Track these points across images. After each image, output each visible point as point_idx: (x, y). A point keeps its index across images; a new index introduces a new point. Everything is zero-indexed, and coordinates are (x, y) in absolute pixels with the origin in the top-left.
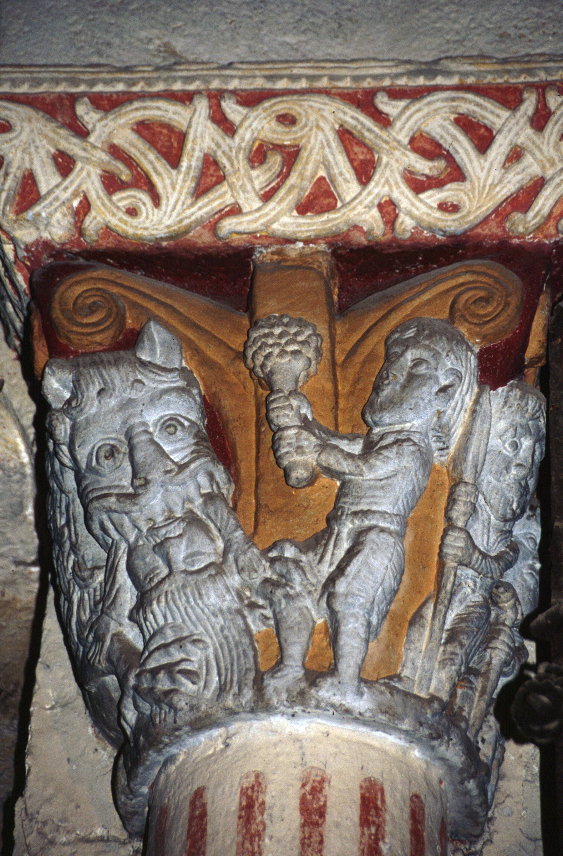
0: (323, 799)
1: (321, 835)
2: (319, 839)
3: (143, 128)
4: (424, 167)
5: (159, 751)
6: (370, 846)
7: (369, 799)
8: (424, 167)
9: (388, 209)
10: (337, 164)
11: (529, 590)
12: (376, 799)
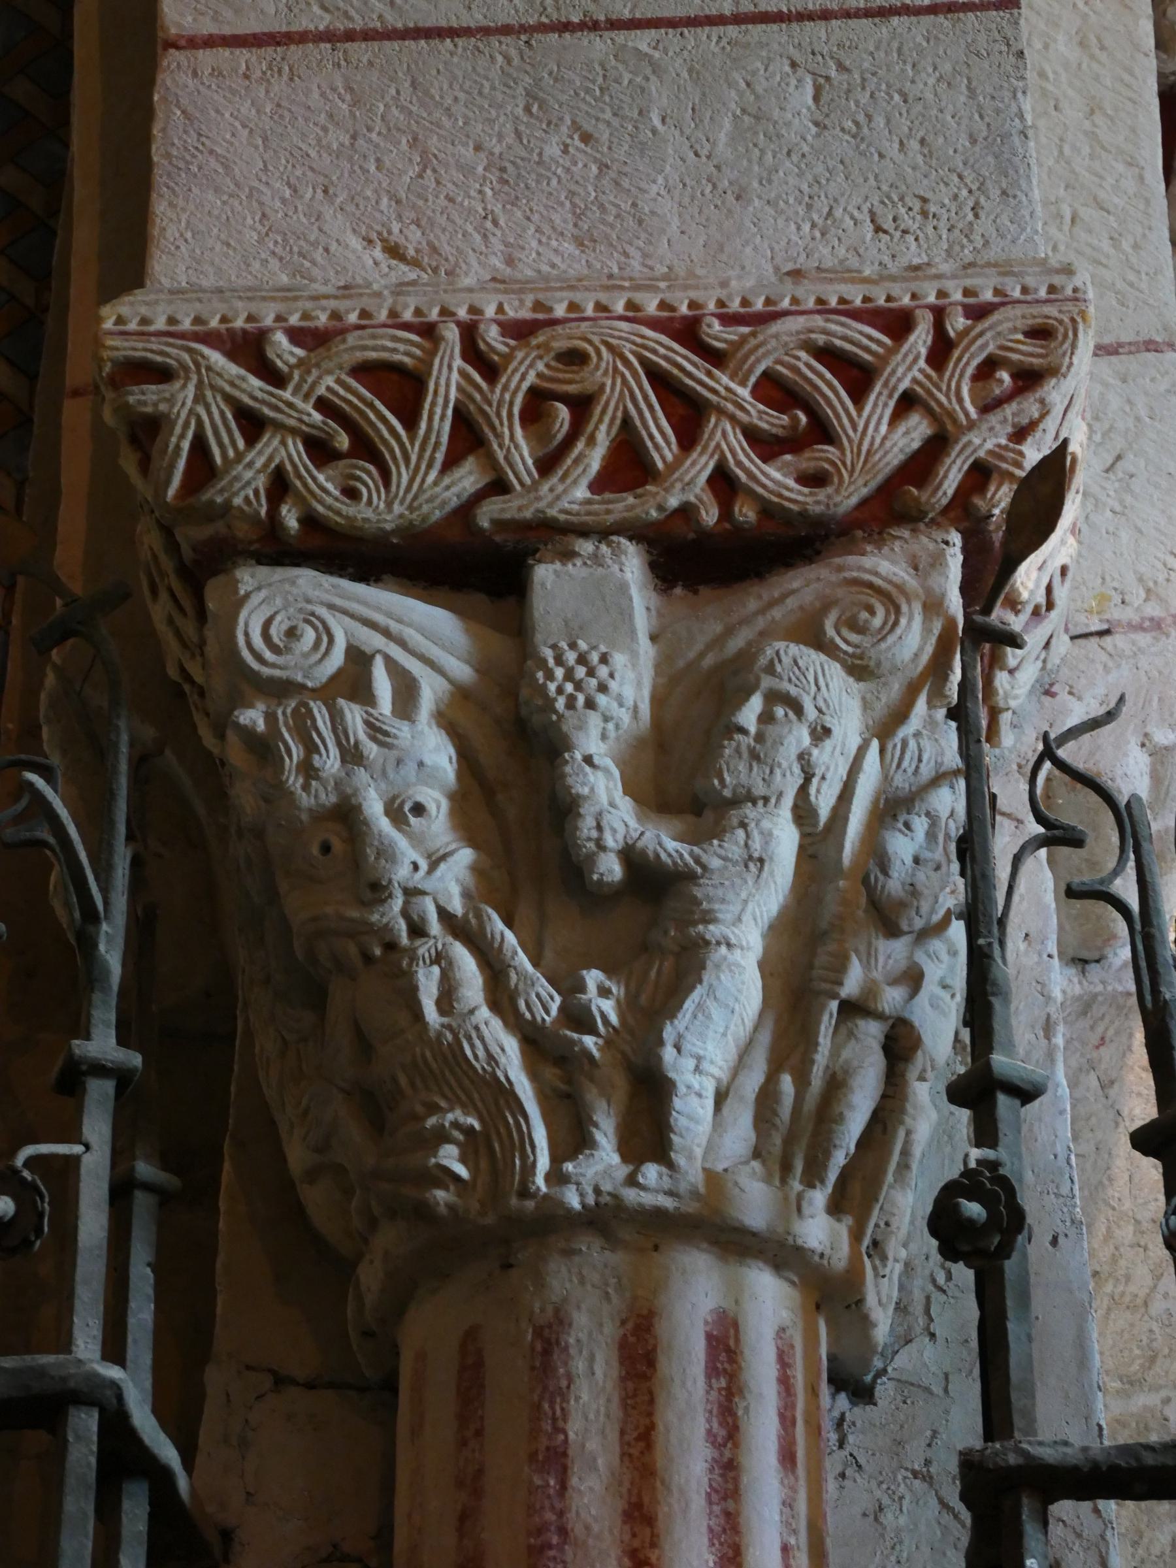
0: (651, 1341)
1: (651, 1393)
2: (646, 1398)
3: (365, 371)
4: (771, 421)
5: (720, 1390)
6: (720, 1405)
7: (717, 1339)
8: (771, 421)
9: (723, 482)
10: (503, 1050)
11: (994, 994)
12: (727, 1337)
